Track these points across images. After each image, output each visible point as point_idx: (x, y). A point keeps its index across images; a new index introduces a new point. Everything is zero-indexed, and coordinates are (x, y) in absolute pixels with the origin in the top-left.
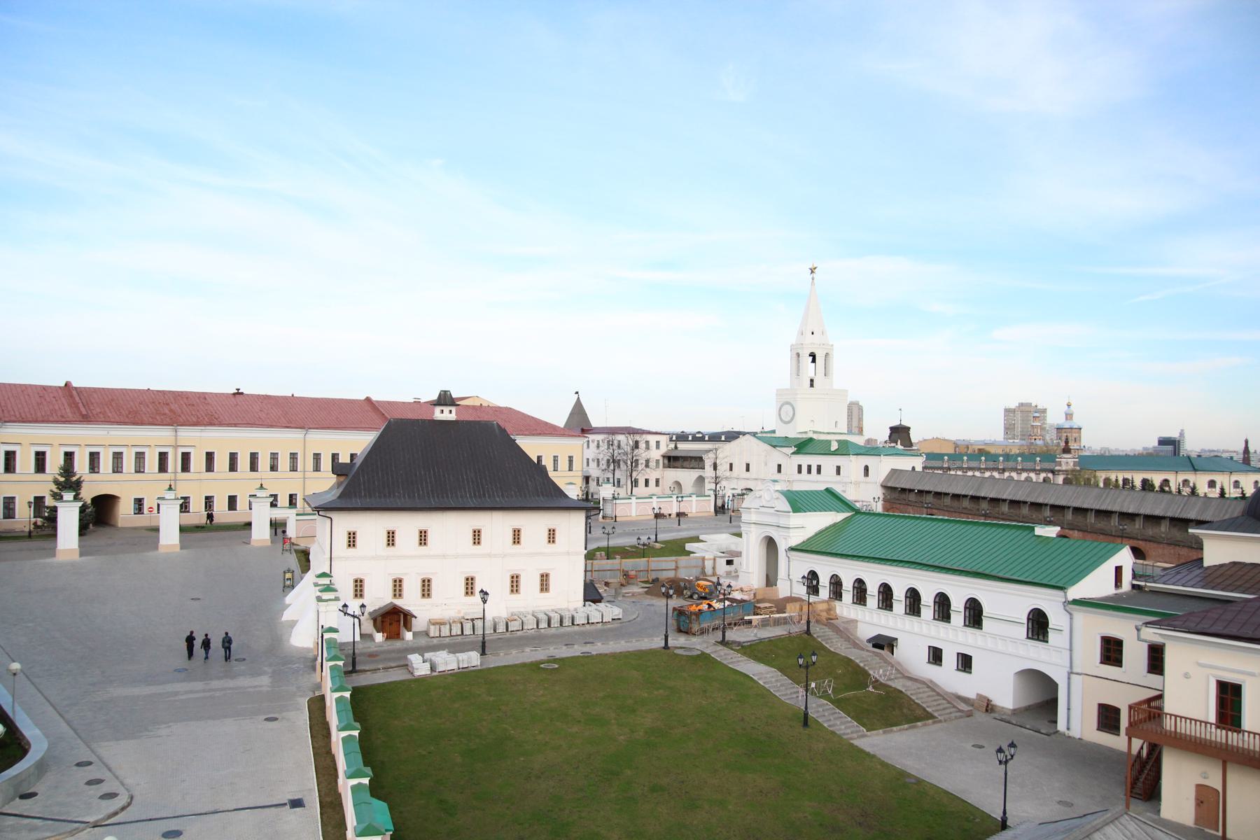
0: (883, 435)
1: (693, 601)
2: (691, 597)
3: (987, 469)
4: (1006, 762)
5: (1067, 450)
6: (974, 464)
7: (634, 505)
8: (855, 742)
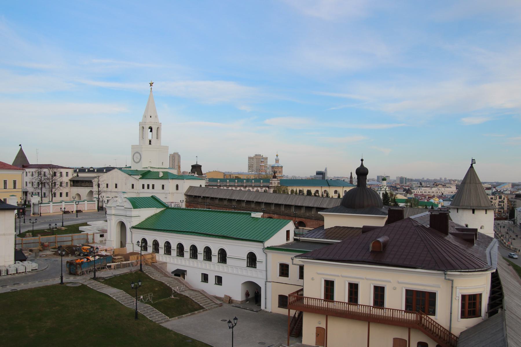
0: (189, 170)
1: (79, 257)
2: (79, 255)
3: (238, 186)
4: (233, 327)
5: (275, 177)
6: (232, 184)
7: (51, 207)
8: (162, 325)
